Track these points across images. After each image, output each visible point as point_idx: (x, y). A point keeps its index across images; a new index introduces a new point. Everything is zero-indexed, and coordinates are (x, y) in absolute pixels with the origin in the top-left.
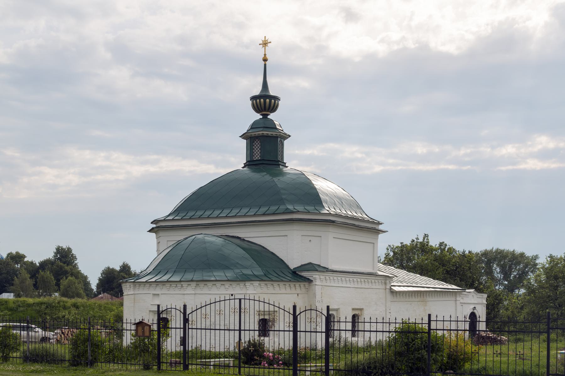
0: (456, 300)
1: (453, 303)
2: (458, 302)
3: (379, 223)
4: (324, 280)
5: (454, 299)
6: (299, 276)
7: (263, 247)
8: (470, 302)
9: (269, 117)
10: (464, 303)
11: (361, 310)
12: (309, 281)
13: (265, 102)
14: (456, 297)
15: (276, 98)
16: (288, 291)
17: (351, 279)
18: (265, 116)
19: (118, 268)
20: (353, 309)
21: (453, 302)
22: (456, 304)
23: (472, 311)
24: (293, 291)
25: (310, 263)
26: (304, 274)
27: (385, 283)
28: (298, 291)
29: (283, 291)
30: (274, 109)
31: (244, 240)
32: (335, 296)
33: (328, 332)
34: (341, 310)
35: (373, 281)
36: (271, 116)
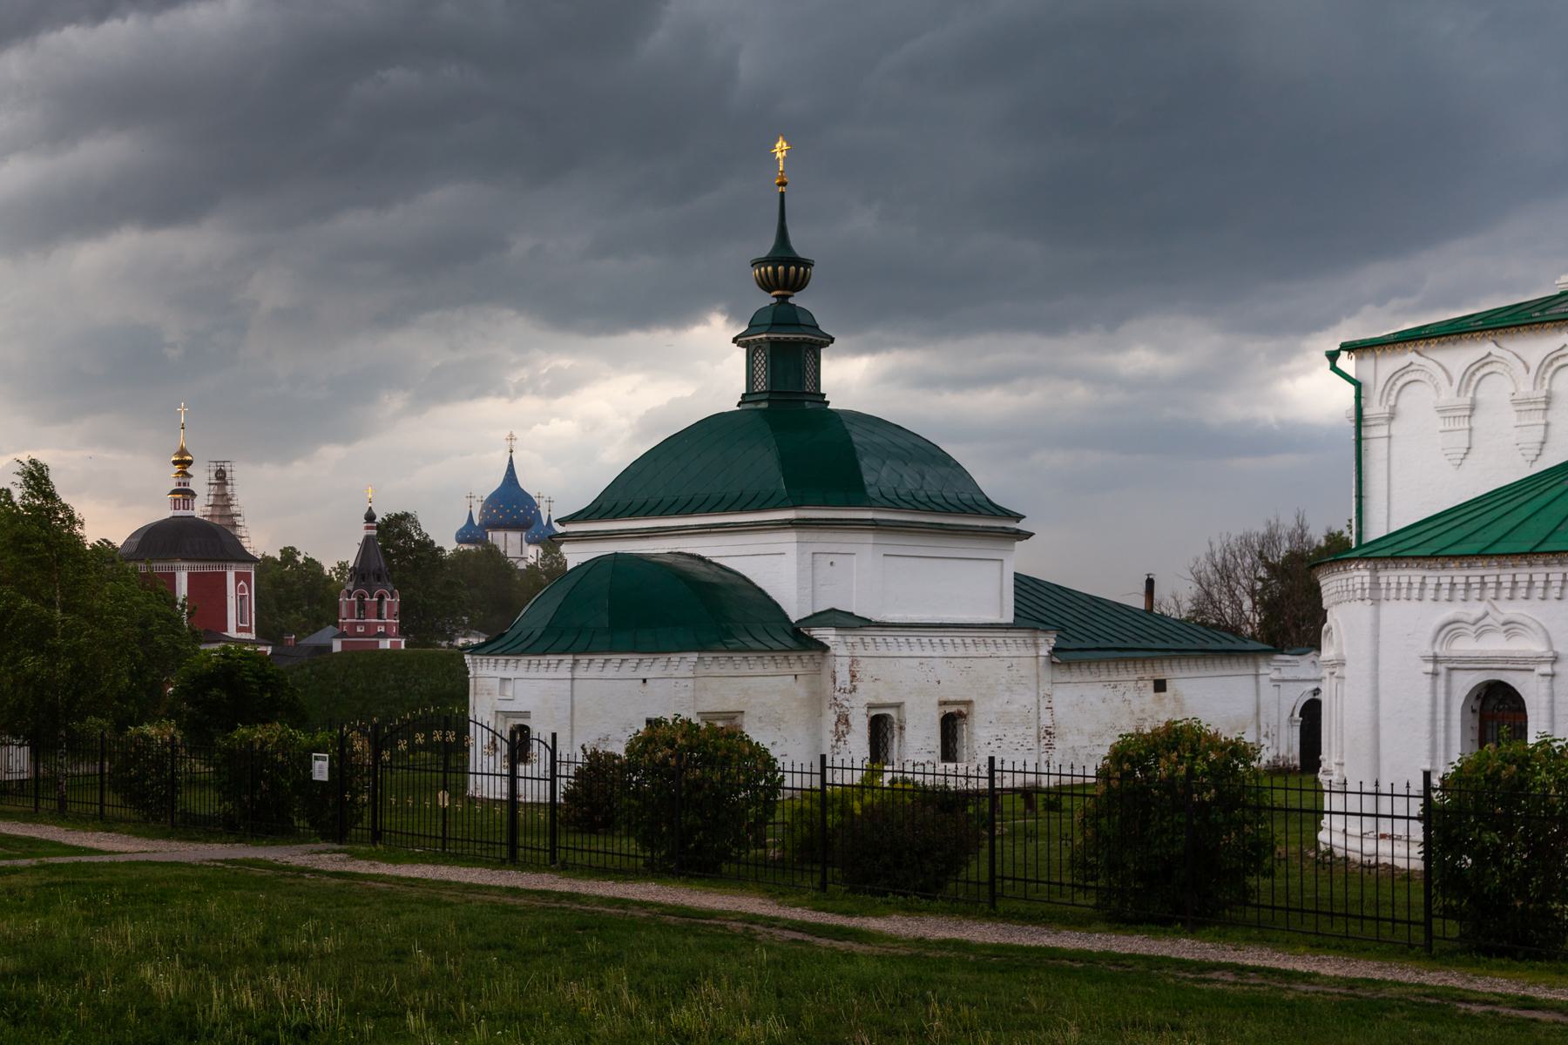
0: (1257, 675)
1: (1249, 682)
2: (1263, 680)
3: (1019, 517)
4: (872, 646)
5: (1252, 671)
6: (797, 639)
7: (744, 578)
8: (1302, 676)
9: (791, 300)
10: (1284, 681)
11: (969, 703)
12: (824, 648)
13: (787, 271)
14: (1257, 667)
15: (808, 264)
16: (772, 669)
17: (936, 640)
18: (783, 299)
19: (620, 749)
20: (943, 703)
21: (1250, 681)
22: (1257, 682)
23: (1310, 696)
24: (784, 669)
25: (833, 610)
26: (817, 633)
27: (1036, 645)
28: (797, 669)
29: (759, 670)
30: (799, 284)
31: (710, 562)
32: (912, 681)
33: (992, 778)
34: (908, 706)
35: (1000, 641)
36: (797, 300)
